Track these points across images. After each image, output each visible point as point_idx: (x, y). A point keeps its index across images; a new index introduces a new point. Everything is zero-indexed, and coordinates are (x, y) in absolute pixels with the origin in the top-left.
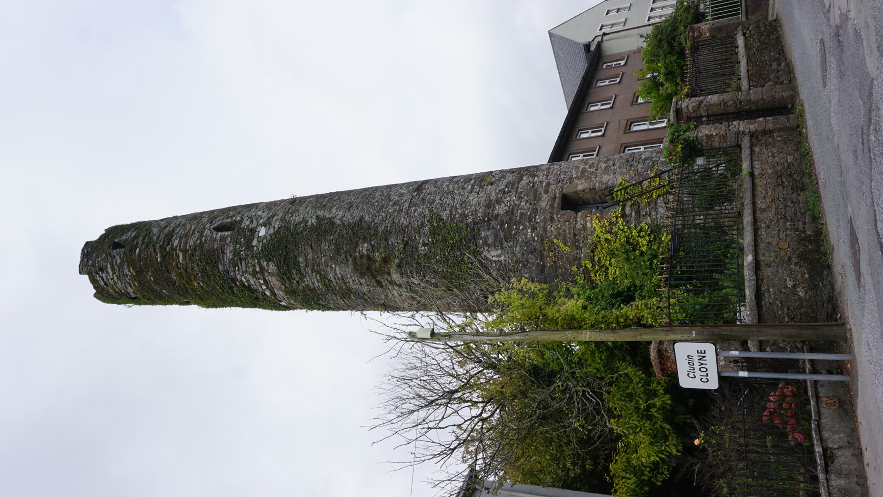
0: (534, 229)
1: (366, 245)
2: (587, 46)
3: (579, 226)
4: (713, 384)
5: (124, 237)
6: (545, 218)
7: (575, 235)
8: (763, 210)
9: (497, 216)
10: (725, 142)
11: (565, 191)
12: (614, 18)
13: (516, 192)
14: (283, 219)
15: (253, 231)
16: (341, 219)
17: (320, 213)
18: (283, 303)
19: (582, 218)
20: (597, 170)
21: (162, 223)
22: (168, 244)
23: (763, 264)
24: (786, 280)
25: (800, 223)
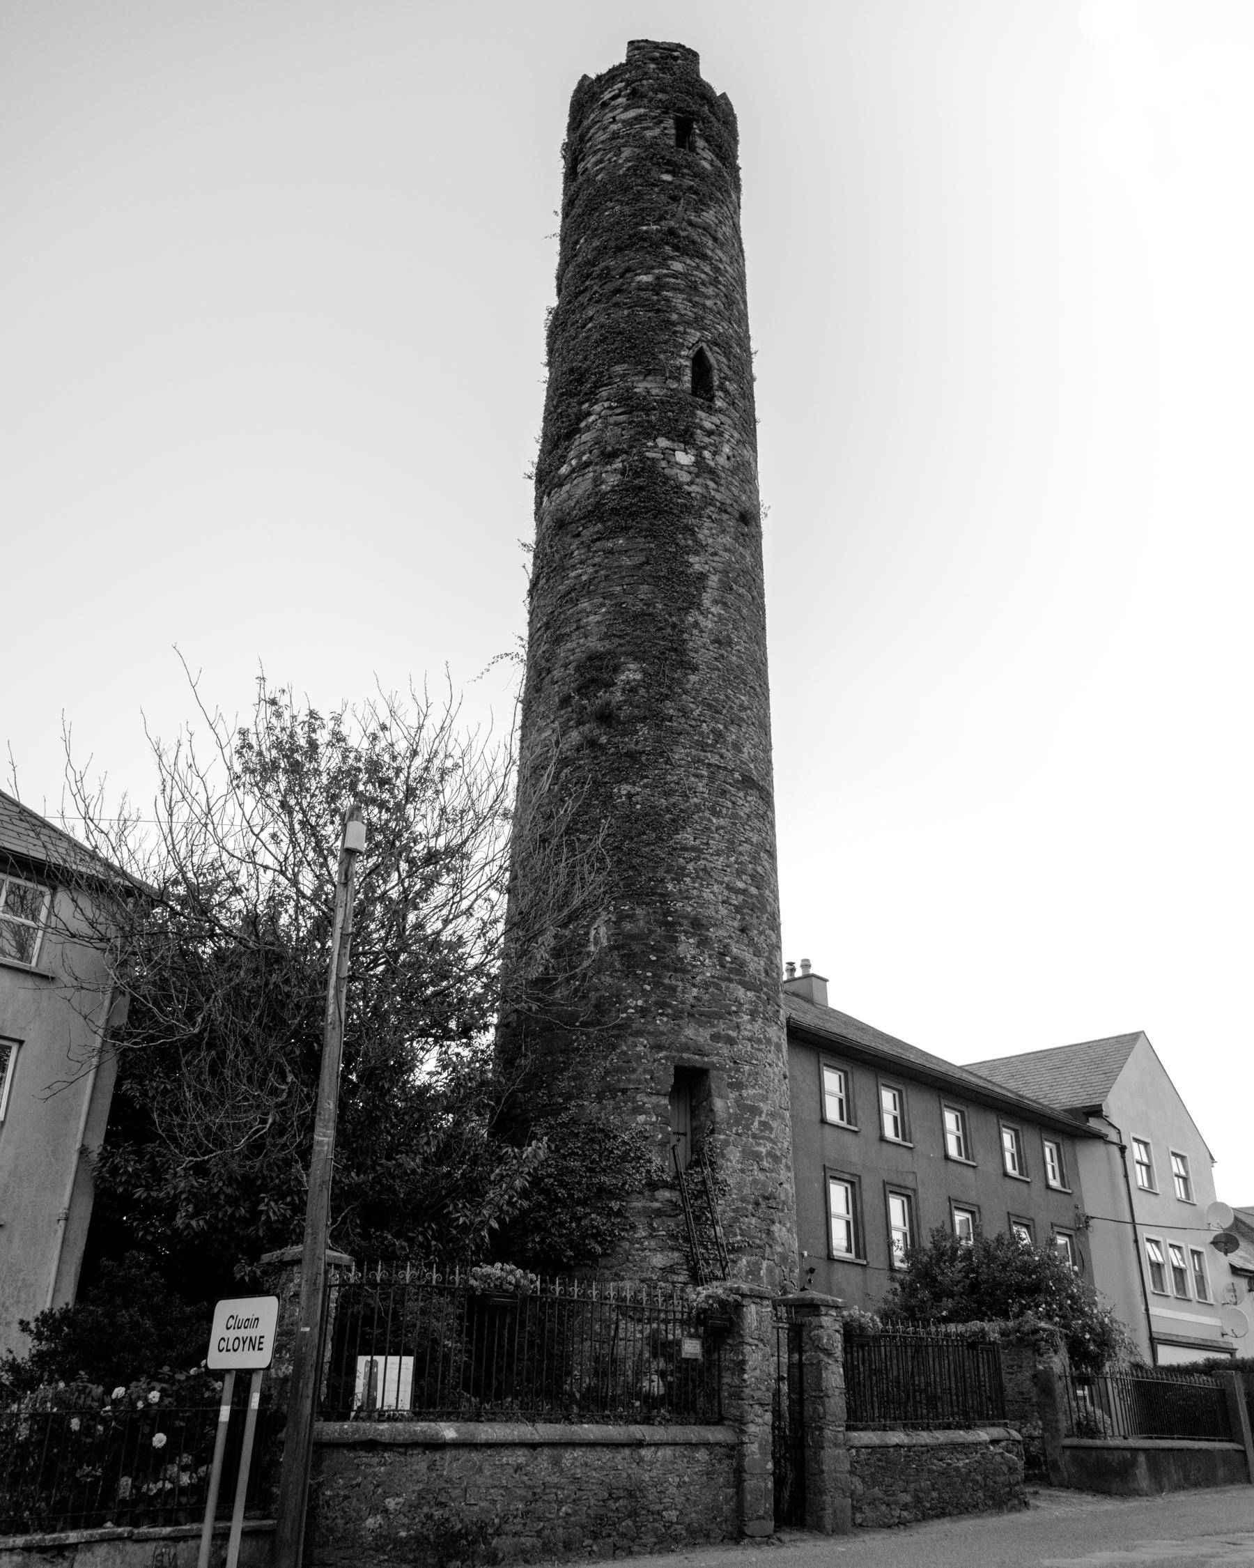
0: (643, 1012)
2: (1096, 1111)
3: (641, 1098)
5: (701, 143)
6: (663, 1033)
7: (624, 1091)
8: (556, 1462)
9: (674, 940)
10: (731, 1395)
11: (713, 1073)
14: (708, 501)
15: (685, 438)
16: (696, 624)
17: (713, 580)
18: (545, 499)
19: (656, 1107)
20: (754, 1136)
21: (727, 230)
23: (438, 1455)
24: (398, 1495)
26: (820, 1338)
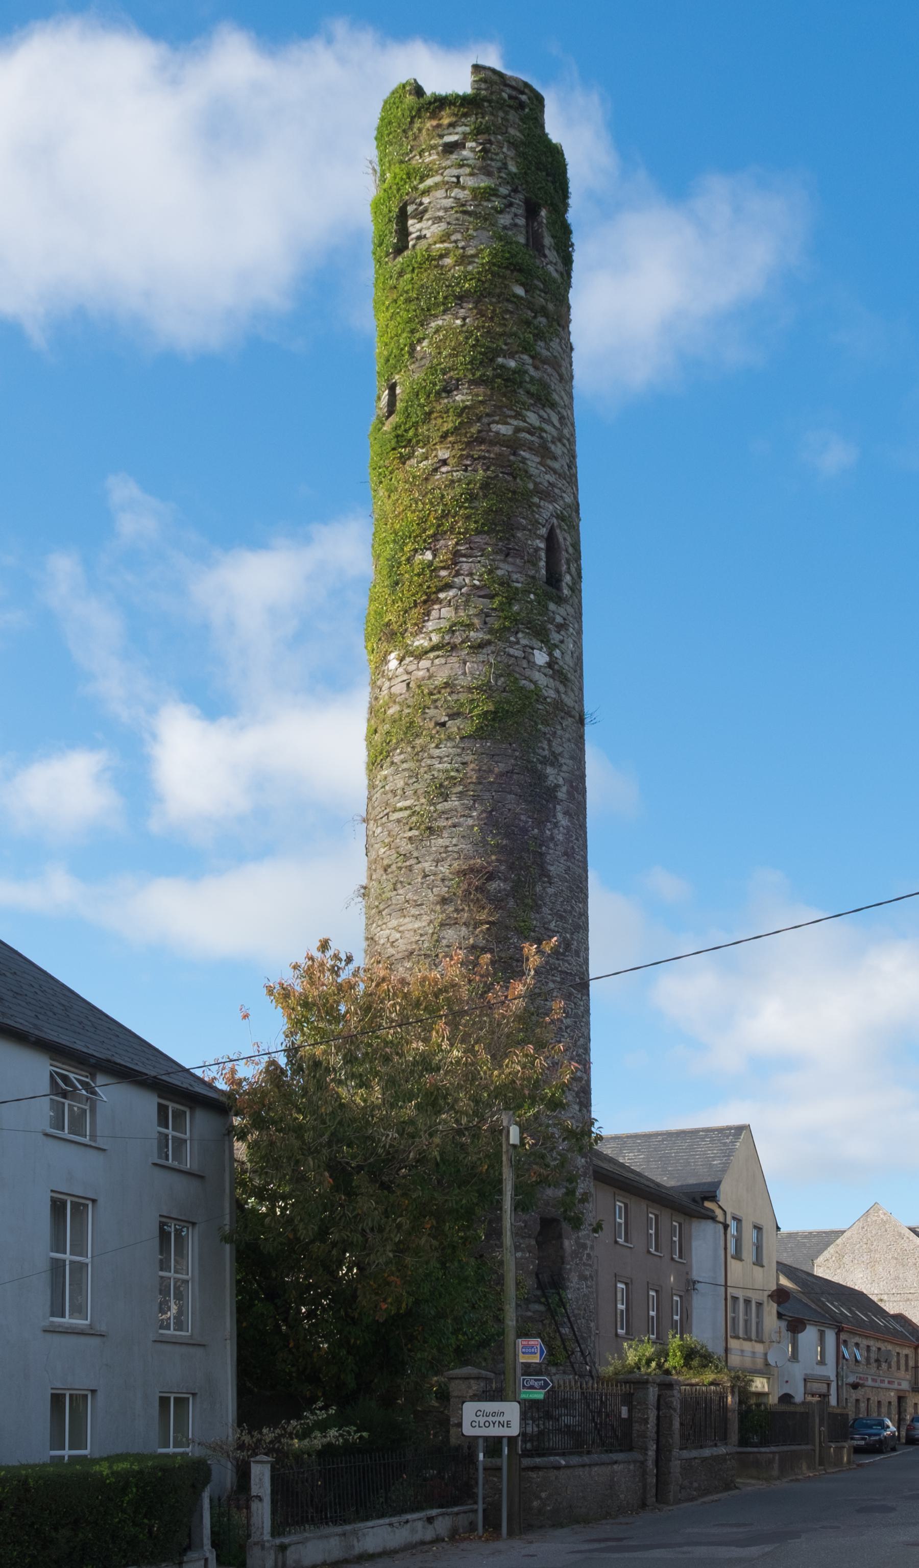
4: (468, 1430)
12: (749, 1236)
26: (672, 1402)
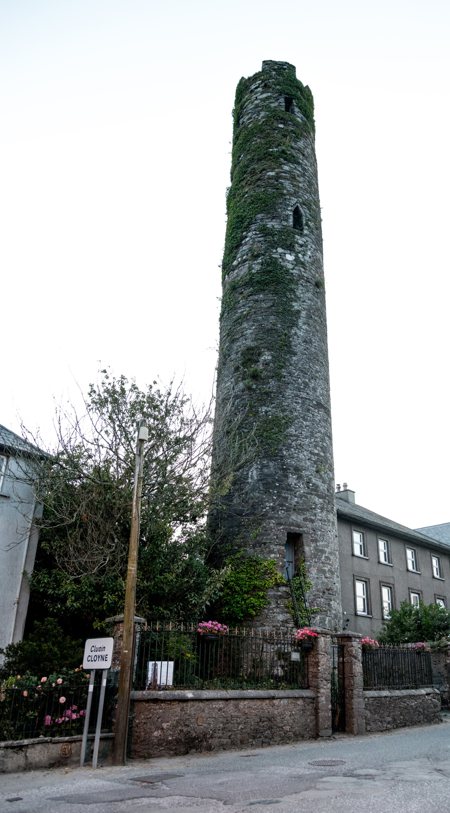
0: (273, 508)
1: (270, 358)
5: (296, 110)
6: (282, 518)
7: (265, 544)
8: (237, 707)
9: (287, 477)
10: (313, 677)
11: (304, 535)
13: (307, 493)
14: (301, 277)
15: (290, 248)
16: (296, 334)
17: (303, 314)
19: (279, 550)
20: (323, 563)
22: (285, 159)
24: (168, 722)
25: (221, 735)
26: (352, 651)
